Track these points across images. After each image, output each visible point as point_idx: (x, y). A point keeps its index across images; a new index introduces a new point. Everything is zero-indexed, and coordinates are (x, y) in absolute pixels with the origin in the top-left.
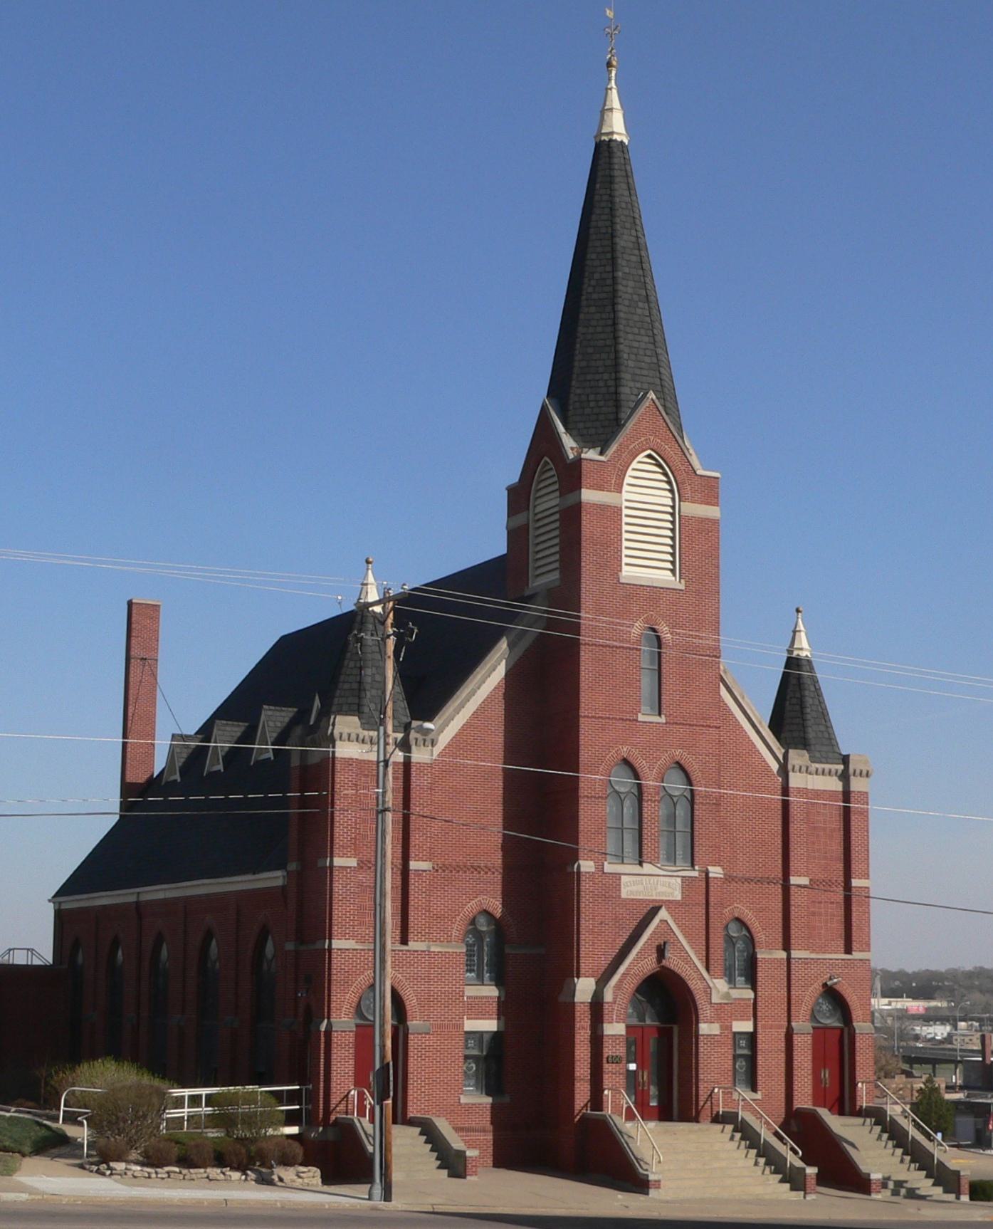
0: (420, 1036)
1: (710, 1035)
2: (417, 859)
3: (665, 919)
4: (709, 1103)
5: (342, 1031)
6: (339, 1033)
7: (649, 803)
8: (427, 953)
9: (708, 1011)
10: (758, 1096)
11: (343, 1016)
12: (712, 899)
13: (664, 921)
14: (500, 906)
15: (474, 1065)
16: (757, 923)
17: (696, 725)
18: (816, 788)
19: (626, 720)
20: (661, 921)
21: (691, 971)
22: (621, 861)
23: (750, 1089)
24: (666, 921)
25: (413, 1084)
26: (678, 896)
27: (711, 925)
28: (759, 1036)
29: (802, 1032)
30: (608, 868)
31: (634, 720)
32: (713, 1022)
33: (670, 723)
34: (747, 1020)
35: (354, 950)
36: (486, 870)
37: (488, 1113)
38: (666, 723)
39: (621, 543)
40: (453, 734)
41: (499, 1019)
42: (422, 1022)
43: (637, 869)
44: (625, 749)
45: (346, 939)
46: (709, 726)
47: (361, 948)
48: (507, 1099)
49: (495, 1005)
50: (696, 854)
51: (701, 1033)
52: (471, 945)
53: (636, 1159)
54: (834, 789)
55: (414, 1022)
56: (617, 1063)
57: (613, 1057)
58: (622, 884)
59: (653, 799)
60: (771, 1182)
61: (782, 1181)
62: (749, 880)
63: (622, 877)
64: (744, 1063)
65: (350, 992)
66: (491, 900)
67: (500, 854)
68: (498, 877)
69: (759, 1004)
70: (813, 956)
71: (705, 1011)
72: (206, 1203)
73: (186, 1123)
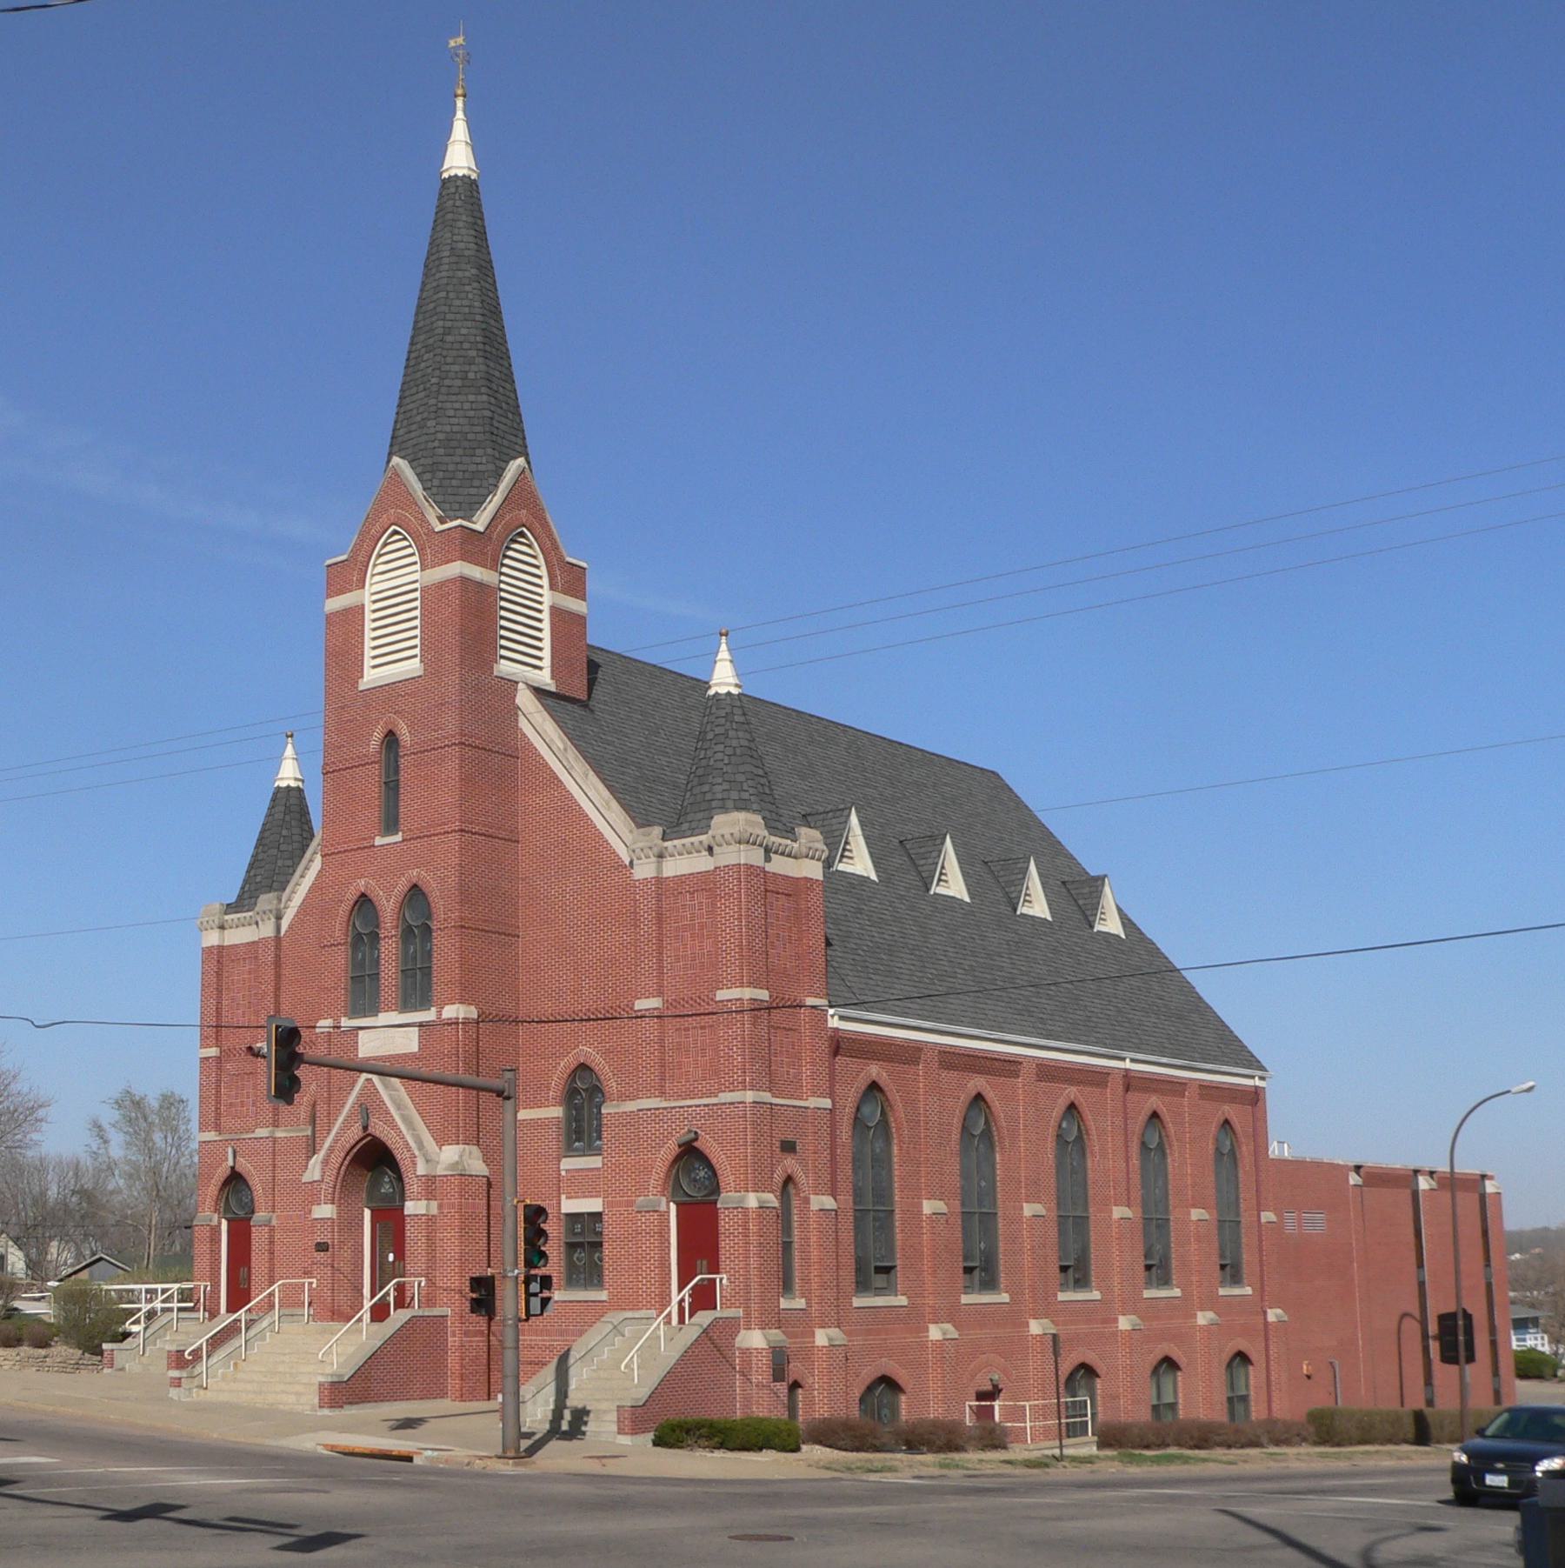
1: (417, 1215)
7: (387, 940)
9: (415, 1186)
16: (607, 1068)
17: (434, 835)
18: (678, 874)
26: (414, 1047)
29: (646, 1209)
32: (420, 1200)
34: (596, 1196)
36: (311, 1044)
38: (403, 841)
39: (421, 624)
63: (361, 1033)
70: (665, 1104)
71: (412, 1186)
72: (925, 1449)
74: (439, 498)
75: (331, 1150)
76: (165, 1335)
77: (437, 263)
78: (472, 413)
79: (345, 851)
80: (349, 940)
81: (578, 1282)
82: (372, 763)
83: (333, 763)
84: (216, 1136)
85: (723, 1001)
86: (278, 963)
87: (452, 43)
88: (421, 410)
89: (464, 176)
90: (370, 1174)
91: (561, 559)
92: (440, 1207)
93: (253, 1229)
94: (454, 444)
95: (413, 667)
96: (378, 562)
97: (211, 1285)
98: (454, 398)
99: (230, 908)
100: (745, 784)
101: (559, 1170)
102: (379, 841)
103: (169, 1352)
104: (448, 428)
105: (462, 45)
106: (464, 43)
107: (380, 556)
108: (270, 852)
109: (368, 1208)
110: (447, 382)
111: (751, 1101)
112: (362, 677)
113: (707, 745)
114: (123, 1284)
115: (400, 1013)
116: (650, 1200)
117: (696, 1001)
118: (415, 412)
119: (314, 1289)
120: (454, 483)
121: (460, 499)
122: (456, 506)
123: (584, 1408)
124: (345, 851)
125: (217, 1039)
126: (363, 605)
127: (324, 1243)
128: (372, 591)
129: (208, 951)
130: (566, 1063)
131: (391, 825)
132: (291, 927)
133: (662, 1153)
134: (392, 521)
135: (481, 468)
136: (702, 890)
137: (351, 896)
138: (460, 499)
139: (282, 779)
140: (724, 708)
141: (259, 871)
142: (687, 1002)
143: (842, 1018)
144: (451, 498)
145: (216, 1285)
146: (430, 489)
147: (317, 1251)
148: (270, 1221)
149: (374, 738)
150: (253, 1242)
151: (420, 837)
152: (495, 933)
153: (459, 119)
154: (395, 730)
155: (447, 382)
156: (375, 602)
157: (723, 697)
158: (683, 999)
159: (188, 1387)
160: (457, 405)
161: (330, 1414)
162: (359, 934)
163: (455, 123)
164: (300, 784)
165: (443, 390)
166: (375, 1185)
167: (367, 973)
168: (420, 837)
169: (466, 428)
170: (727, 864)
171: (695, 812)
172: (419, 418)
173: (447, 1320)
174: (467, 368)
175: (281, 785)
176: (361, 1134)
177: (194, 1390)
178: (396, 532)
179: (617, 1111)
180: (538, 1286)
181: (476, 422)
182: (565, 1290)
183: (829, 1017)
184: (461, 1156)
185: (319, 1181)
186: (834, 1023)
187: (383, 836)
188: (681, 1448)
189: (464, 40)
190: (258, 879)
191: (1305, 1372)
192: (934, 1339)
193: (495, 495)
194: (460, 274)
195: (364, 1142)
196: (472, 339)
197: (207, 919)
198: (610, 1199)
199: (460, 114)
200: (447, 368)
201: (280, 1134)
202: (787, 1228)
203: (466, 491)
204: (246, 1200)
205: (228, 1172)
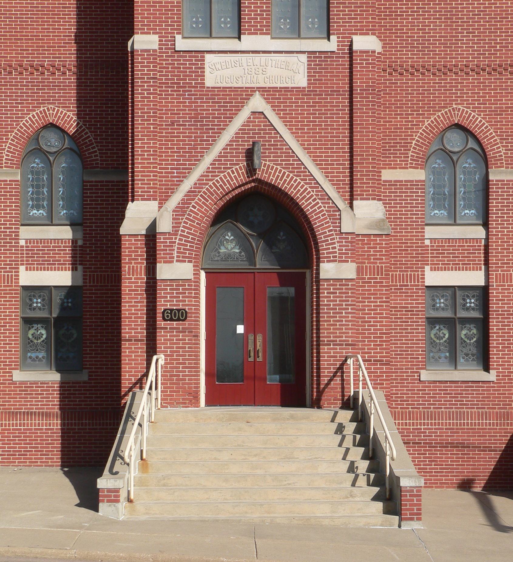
3: (260, 110)
4: (338, 380)
9: (337, 245)
10: (492, 376)
12: (357, 83)
13: (258, 114)
14: (75, 118)
15: (44, 332)
20: (253, 113)
22: (209, 36)
23: (482, 368)
24: (262, 113)
26: (302, 81)
27: (357, 121)
28: (493, 293)
30: (181, 44)
37: (56, 394)
41: (74, 269)
43: (232, 44)
48: (84, 377)
49: (68, 250)
50: (334, 19)
51: (322, 276)
52: (38, 173)
53: (117, 454)
56: (179, 320)
57: (172, 310)
58: (206, 66)
60: (357, 499)
61: (376, 498)
62: (479, 70)
63: (208, 57)
64: (475, 331)
66: (61, 109)
67: (73, 48)
68: (71, 79)
69: (493, 246)
75: (191, 195)
92: (359, 271)
127: (179, 310)
147: (164, 319)
176: (243, 178)
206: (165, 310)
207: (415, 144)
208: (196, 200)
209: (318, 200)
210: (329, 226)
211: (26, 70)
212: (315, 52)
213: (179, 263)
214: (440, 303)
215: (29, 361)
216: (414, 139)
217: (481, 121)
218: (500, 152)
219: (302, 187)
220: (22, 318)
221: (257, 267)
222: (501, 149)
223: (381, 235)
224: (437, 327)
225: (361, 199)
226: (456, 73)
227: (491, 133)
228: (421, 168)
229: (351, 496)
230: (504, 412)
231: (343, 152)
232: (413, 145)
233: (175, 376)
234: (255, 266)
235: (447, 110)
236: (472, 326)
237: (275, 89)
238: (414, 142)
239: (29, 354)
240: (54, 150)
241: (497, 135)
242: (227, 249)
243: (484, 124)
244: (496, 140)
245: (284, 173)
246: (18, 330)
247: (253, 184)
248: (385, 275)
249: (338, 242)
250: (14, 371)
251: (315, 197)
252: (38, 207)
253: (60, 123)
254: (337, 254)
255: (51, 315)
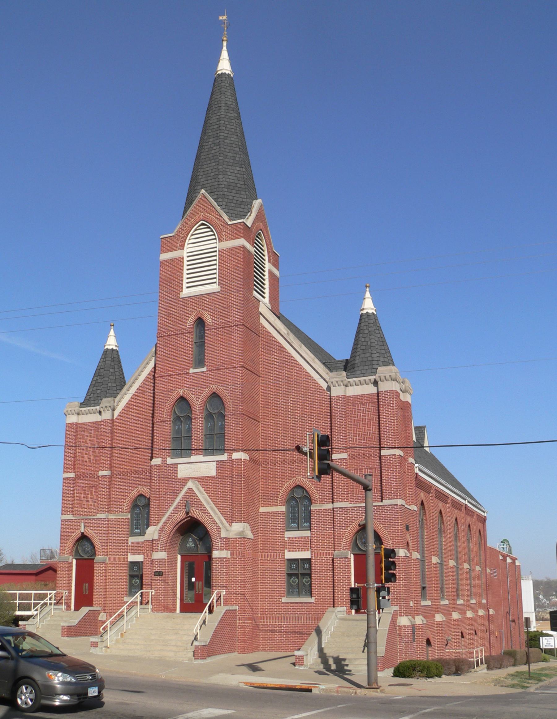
0: (100, 564)
2: (103, 470)
5: (63, 562)
6: (65, 563)
8: (106, 519)
9: (219, 543)
11: (65, 554)
13: (190, 489)
15: (138, 581)
17: (227, 368)
18: (356, 394)
19: (183, 374)
20: (189, 489)
21: (208, 518)
25: (96, 590)
26: (213, 473)
30: (170, 461)
31: (187, 373)
33: (210, 371)
35: (71, 520)
38: (207, 371)
40: (126, 402)
42: (103, 557)
44: (182, 391)
45: (68, 514)
46: (235, 367)
47: (75, 518)
54: (370, 392)
55: (100, 557)
57: (157, 572)
58: (178, 470)
59: (198, 417)
60: (189, 650)
63: (179, 465)
65: (69, 542)
66: (145, 488)
71: (217, 542)
73: (17, 608)
74: (227, 211)
75: (165, 523)
76: (47, 618)
77: (218, 108)
78: (238, 175)
79: (170, 375)
80: (172, 419)
81: (293, 593)
82: (188, 333)
83: (164, 332)
84: (72, 517)
85: (385, 456)
86: (112, 432)
87: (221, 18)
88: (214, 170)
89: (228, 74)
90: (181, 537)
91: (272, 249)
92: (232, 554)
93: (96, 564)
94: (232, 187)
95: (215, 288)
96: (191, 238)
97: (68, 592)
98: (230, 167)
99: (82, 405)
100: (385, 355)
101: (284, 538)
102: (192, 371)
103: (63, 626)
104: (228, 180)
105: (225, 19)
106: (227, 19)
107: (192, 235)
108: (105, 379)
109: (180, 554)
110: (226, 160)
111: (401, 504)
112: (182, 292)
113: (365, 335)
114: (25, 590)
115: (203, 456)
116: (342, 552)
117: (366, 456)
118: (210, 171)
119: (153, 595)
120: (233, 205)
121: (235, 212)
122: (234, 215)
123: (338, 657)
124: (170, 375)
125: (74, 469)
126: (183, 258)
127: (160, 572)
128: (188, 251)
129: (70, 426)
130: (289, 484)
131: (200, 362)
132: (120, 415)
133: (349, 529)
134: (202, 218)
135: (244, 200)
136: (370, 402)
137: (174, 396)
138: (235, 212)
139: (109, 345)
140: (372, 320)
141: (98, 388)
142: (361, 456)
143: (420, 470)
144: (232, 212)
145: (70, 592)
146: (222, 205)
147: (155, 576)
148: (106, 560)
149: (189, 321)
150: (95, 571)
151: (218, 369)
152: (253, 419)
153: (224, 50)
154: (202, 317)
155: (226, 160)
156: (188, 257)
157: (371, 314)
158: (359, 455)
159: (101, 647)
160: (232, 171)
161: (202, 662)
162: (178, 417)
163: (223, 52)
164: (117, 348)
165: (225, 163)
166: (184, 542)
167: (183, 436)
168: (218, 369)
169: (236, 182)
170: (387, 390)
171: (363, 366)
172: (213, 174)
173: (236, 612)
174: (235, 155)
175: (108, 348)
176: (184, 516)
177: (104, 648)
178: (203, 224)
179: (321, 508)
180: (387, 593)
181: (241, 179)
182: (286, 597)
183: (415, 468)
184: (244, 528)
185: (157, 540)
186: (417, 471)
187: (194, 369)
188: (412, 677)
189: (227, 18)
190: (98, 391)
191: (496, 635)
192: (438, 621)
193: (251, 213)
194: (229, 115)
195: (185, 520)
196: (237, 143)
197: (70, 409)
198: (316, 552)
199: (225, 48)
200: (226, 154)
201: (111, 517)
202: (423, 565)
203: (238, 209)
204: (88, 550)
205: (80, 535)
206: (155, 571)
207: (281, 495)
208: (167, 526)
209: (212, 524)
210: (217, 535)
211: (133, 473)
212: (218, 461)
213: (160, 552)
214: (293, 566)
215: (132, 593)
216: (280, 493)
217: (308, 483)
218: (317, 497)
219: (206, 519)
220: (130, 575)
221: (199, 553)
222: (317, 495)
223: (241, 538)
224: (293, 578)
225: (235, 522)
226: (298, 463)
227: (313, 489)
228: (284, 506)
229: (186, 649)
230: (317, 617)
231: (229, 502)
232: (280, 496)
233: (158, 599)
234: (198, 552)
235: (294, 479)
236: (308, 577)
237: (203, 477)
238: (280, 494)
239: (133, 590)
240: (142, 505)
241: (315, 489)
242: (189, 545)
243: (310, 484)
244: (315, 491)
245: (200, 513)
246: (284, 579)
247: (189, 518)
248: (243, 555)
249: (220, 542)
250: (124, 597)
251: (211, 523)
252: (137, 529)
253: (144, 494)
254: (220, 547)
255: (299, 572)
